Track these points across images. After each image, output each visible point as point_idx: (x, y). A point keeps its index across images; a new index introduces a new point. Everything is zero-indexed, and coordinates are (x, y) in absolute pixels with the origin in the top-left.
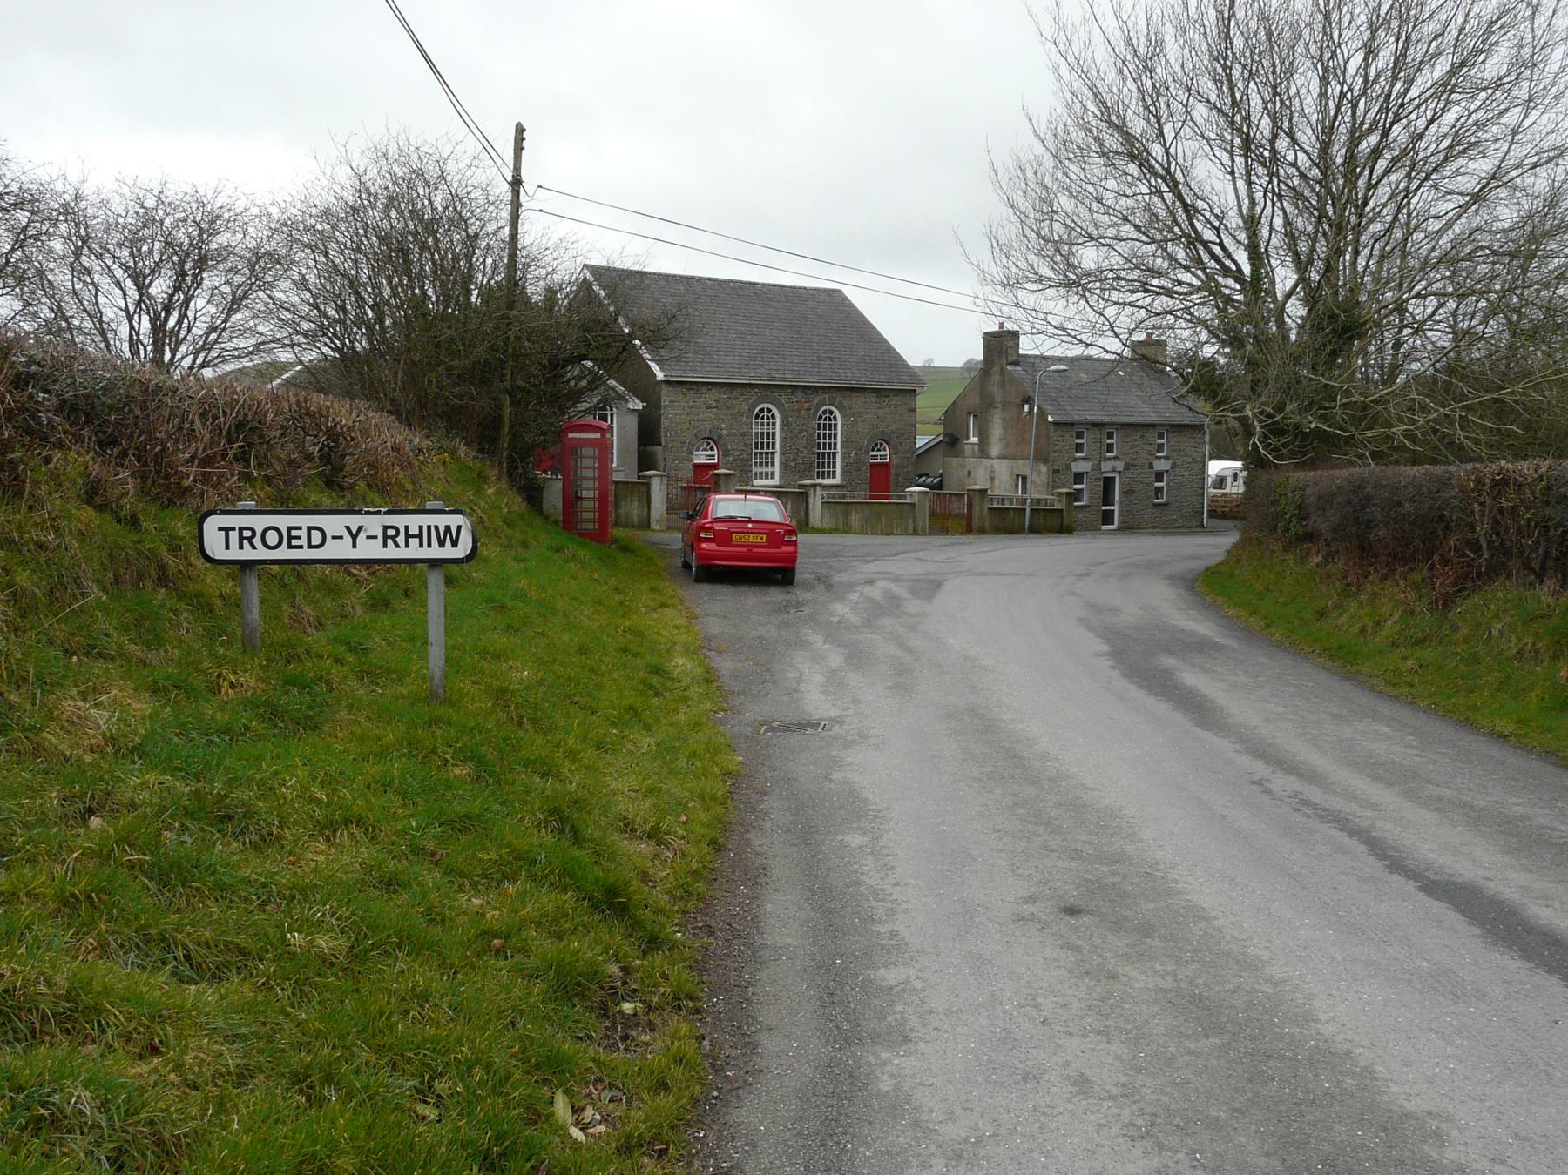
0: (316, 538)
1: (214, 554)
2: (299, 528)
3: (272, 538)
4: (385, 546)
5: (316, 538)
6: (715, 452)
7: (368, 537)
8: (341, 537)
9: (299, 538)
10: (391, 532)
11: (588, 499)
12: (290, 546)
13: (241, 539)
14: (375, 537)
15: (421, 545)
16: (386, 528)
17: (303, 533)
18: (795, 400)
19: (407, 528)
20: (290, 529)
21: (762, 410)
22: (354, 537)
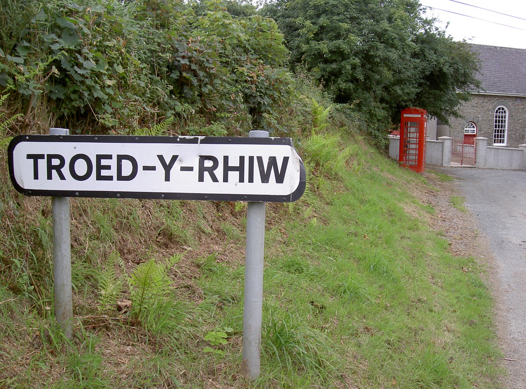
0: (127, 168)
1: (23, 183)
2: (109, 157)
3: (81, 167)
4: (201, 179)
5: (127, 168)
6: (475, 129)
7: (183, 169)
8: (153, 168)
9: (108, 167)
10: (208, 164)
11: (412, 155)
12: (100, 177)
13: (50, 167)
14: (191, 169)
15: (241, 180)
16: (203, 158)
17: (113, 163)
18: (516, 104)
19: (226, 159)
20: (99, 157)
21: (499, 109)
22: (168, 168)
